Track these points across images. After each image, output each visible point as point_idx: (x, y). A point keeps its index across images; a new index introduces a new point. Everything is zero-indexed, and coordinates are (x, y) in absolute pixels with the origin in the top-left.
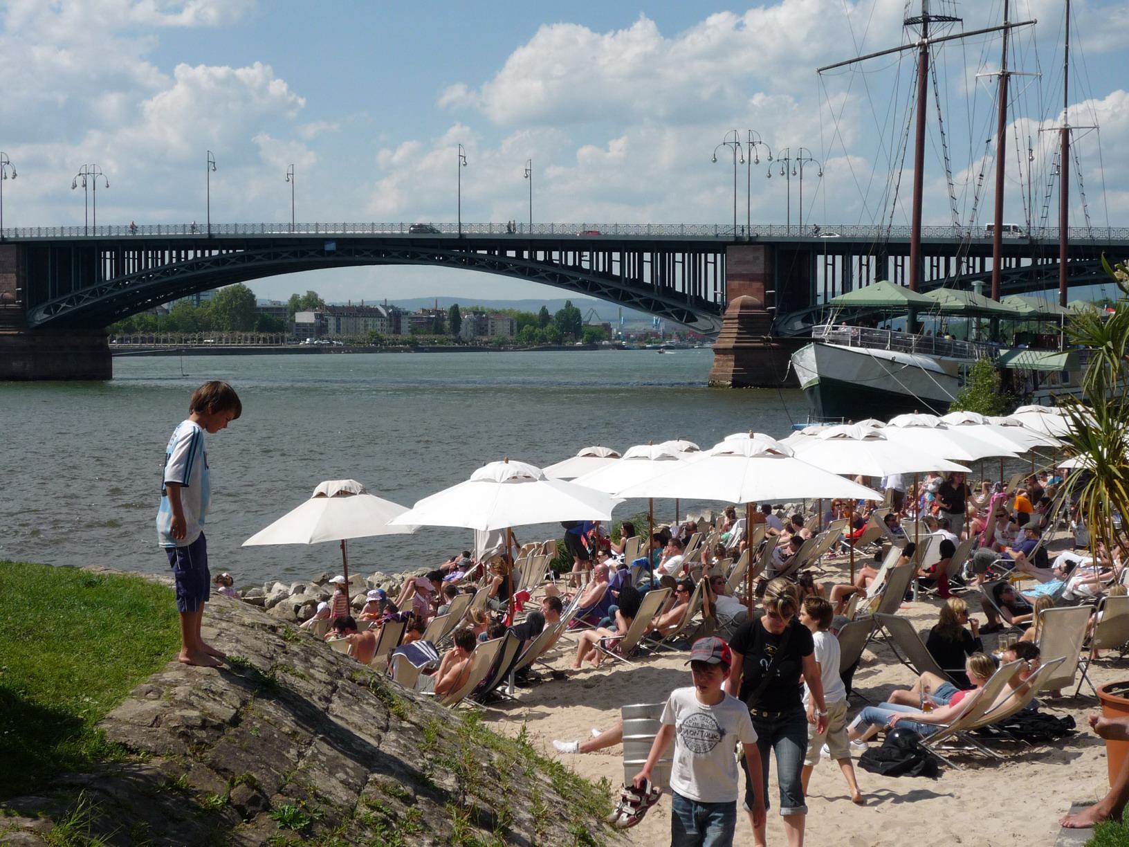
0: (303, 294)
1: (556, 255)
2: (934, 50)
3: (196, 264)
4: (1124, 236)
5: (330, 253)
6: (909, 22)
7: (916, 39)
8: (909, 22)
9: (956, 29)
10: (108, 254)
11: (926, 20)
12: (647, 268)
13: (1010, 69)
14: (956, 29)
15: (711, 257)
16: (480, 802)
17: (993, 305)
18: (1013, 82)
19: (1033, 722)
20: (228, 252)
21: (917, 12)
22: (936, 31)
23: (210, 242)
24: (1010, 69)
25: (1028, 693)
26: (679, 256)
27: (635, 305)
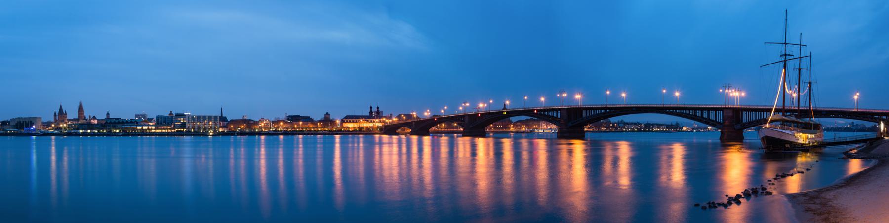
0: (620, 120)
1: (684, 111)
2: (787, 62)
3: (604, 113)
4: (888, 111)
5: (634, 111)
6: (781, 56)
7: (783, 59)
8: (781, 56)
9: (792, 57)
10: (698, 111)
11: (786, 55)
12: (559, 114)
13: (801, 68)
14: (792, 57)
15: (705, 111)
16: (820, 151)
17: (799, 120)
18: (802, 71)
19: (872, 144)
20: (444, 109)
21: (784, 53)
22: (788, 57)
23: (607, 108)
24: (801, 68)
25: (696, 203)
26: (698, 111)
27: (696, 120)
